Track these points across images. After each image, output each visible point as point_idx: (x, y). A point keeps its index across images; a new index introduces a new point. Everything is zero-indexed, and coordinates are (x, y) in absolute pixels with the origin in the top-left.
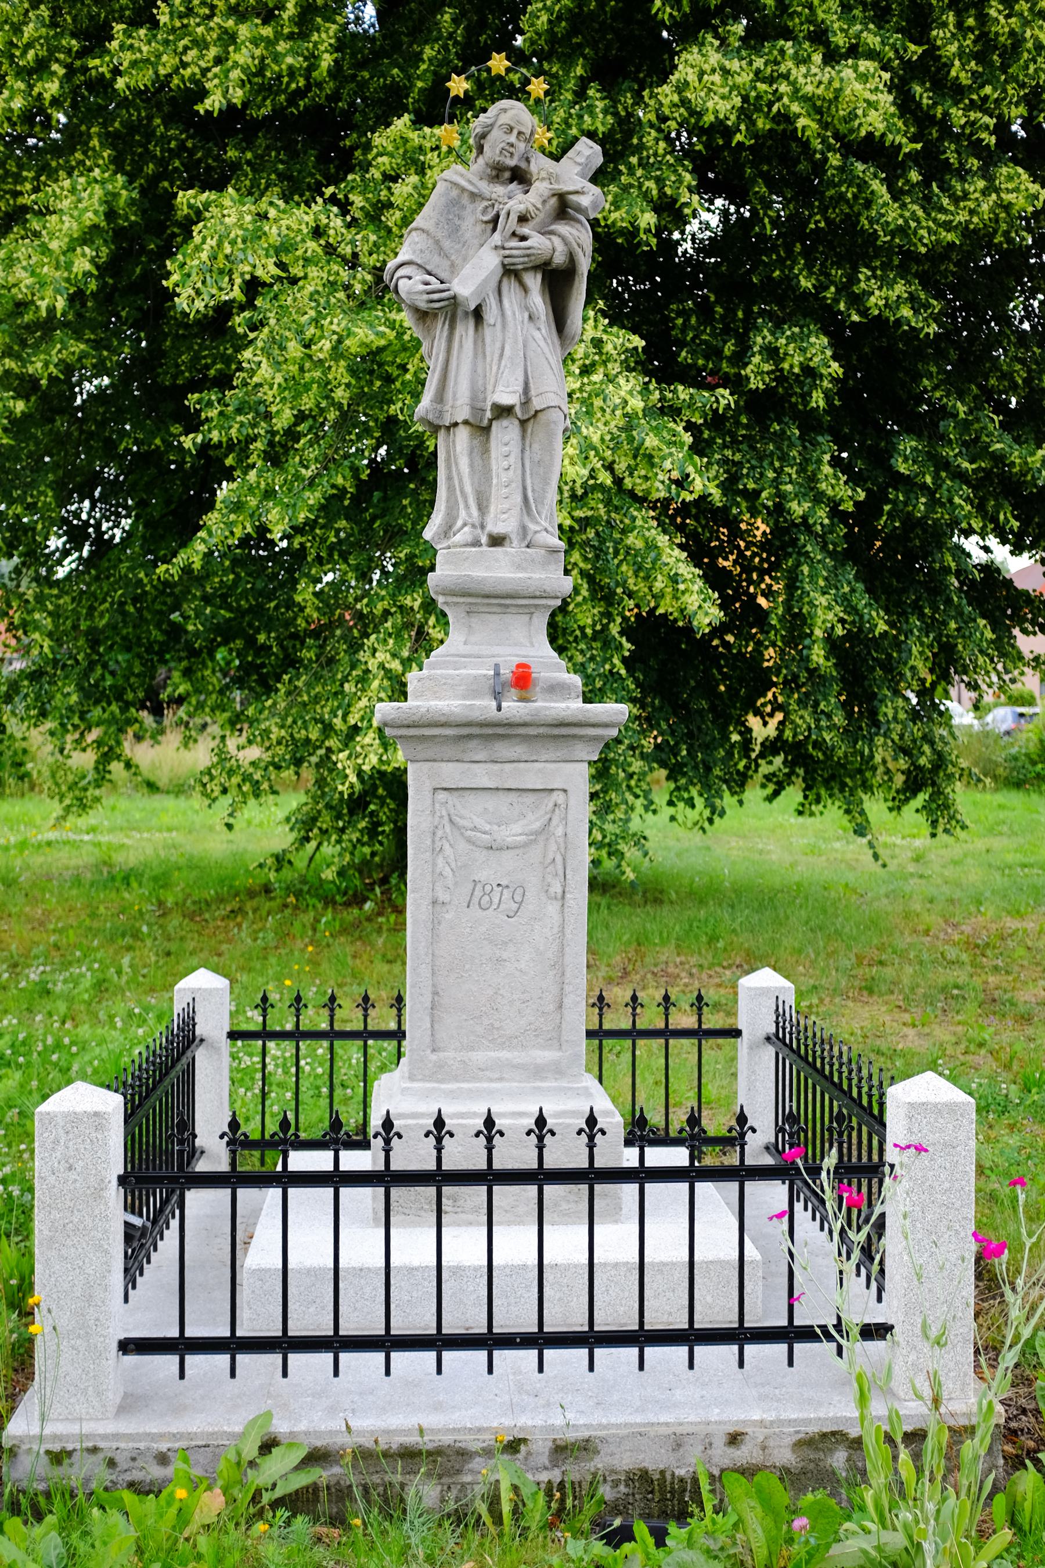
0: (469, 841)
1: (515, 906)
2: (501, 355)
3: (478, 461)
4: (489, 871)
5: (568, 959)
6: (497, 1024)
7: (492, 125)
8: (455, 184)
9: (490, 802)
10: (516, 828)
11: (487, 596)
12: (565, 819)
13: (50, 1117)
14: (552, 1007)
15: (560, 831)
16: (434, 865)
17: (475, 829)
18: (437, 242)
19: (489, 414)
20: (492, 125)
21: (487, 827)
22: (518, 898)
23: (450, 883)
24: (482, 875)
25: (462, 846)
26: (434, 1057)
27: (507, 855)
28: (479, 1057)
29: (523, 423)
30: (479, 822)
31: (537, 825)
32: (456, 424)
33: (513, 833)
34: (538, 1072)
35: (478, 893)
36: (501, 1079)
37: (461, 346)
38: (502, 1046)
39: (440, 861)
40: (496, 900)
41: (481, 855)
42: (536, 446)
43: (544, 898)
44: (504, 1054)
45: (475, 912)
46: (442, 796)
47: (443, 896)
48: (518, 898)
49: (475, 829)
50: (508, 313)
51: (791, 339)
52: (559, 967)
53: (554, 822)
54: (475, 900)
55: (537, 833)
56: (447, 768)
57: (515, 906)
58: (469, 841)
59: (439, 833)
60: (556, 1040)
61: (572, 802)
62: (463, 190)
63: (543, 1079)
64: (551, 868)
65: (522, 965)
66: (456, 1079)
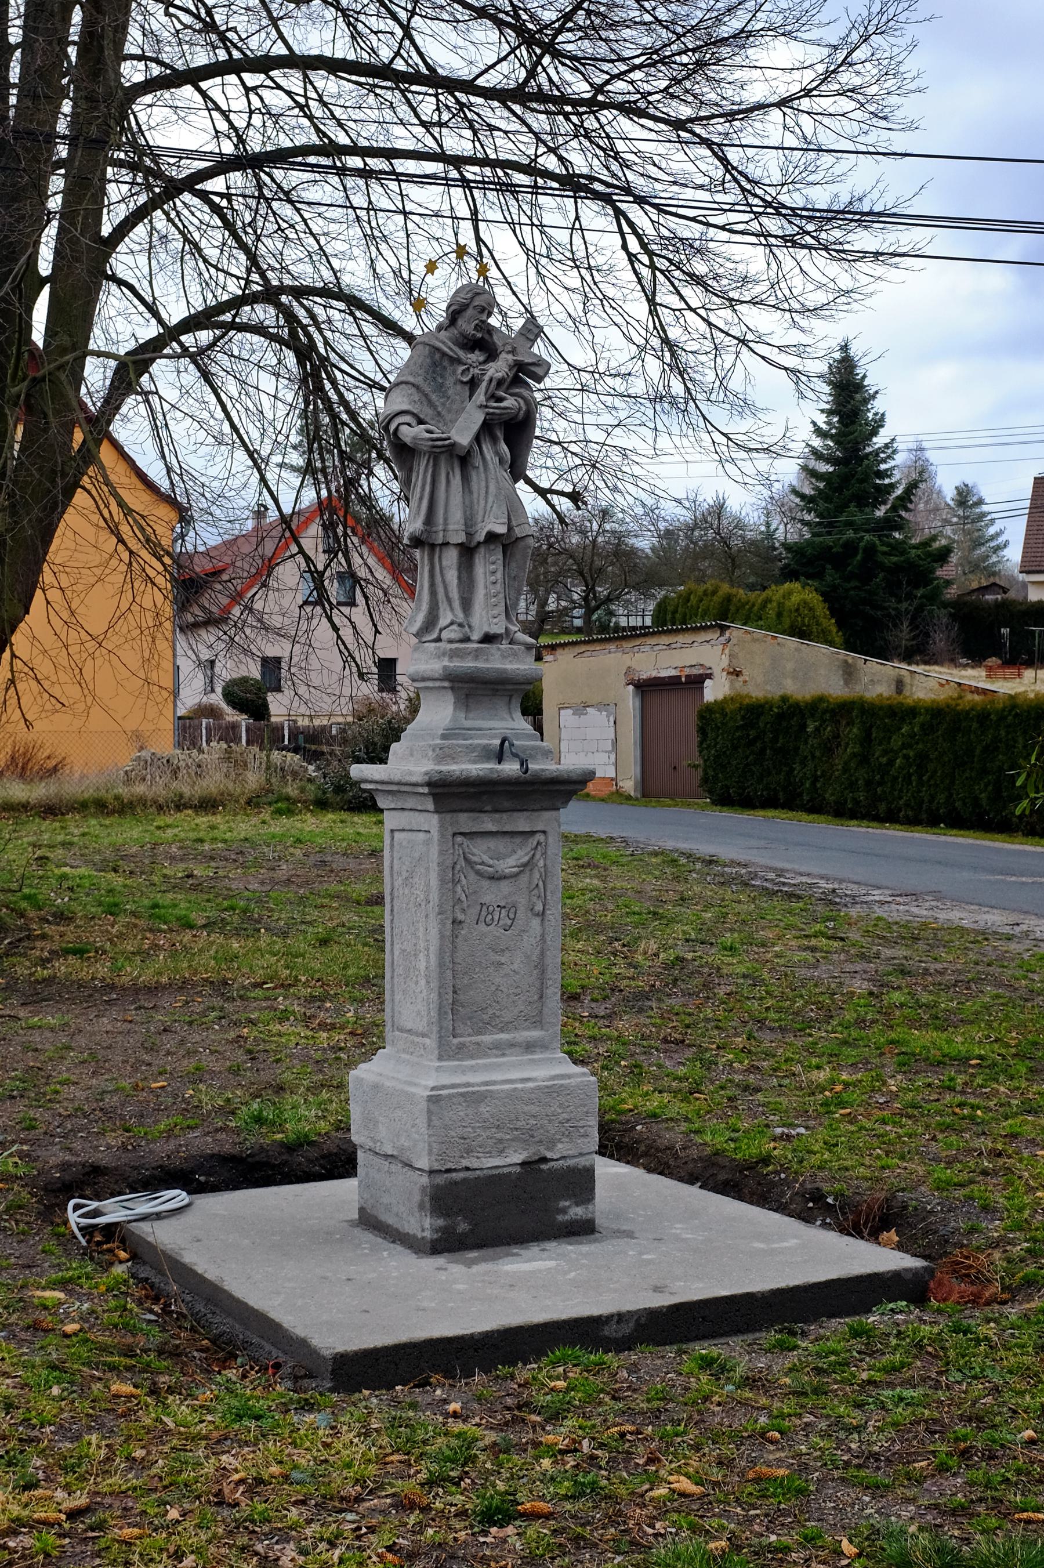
0: (478, 873)
1: (509, 922)
2: (487, 492)
3: (464, 575)
4: (493, 894)
5: (548, 961)
6: (498, 1013)
7: (468, 305)
8: (438, 349)
9: (492, 843)
10: (512, 861)
11: (486, 683)
12: (544, 853)
13: (360, 1080)
14: (536, 997)
15: (541, 863)
16: (455, 892)
17: (483, 863)
18: (426, 395)
19: (482, 539)
20: (468, 305)
21: (491, 862)
22: (512, 916)
23: (465, 905)
24: (486, 899)
25: (472, 876)
26: (456, 1041)
27: (504, 884)
28: (487, 1039)
29: (505, 548)
30: (485, 858)
31: (526, 859)
32: (446, 544)
33: (508, 865)
34: (529, 1047)
35: (484, 913)
36: (504, 1055)
37: (448, 481)
38: (501, 1030)
39: (459, 889)
40: (496, 918)
41: (486, 883)
42: (513, 565)
43: (530, 914)
44: (503, 1036)
45: (482, 926)
46: (459, 839)
47: (461, 917)
48: (512, 916)
49: (483, 863)
50: (488, 457)
51: (775, 549)
52: (541, 968)
53: (538, 856)
54: (482, 918)
55: (525, 865)
56: (463, 817)
57: (509, 922)
58: (478, 873)
59: (458, 867)
60: (538, 1022)
61: (550, 840)
62: (444, 354)
63: (532, 1053)
64: (536, 891)
65: (515, 967)
66: (472, 1057)
